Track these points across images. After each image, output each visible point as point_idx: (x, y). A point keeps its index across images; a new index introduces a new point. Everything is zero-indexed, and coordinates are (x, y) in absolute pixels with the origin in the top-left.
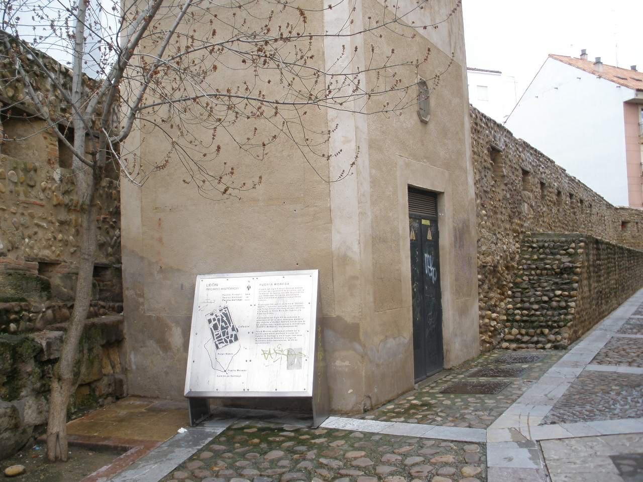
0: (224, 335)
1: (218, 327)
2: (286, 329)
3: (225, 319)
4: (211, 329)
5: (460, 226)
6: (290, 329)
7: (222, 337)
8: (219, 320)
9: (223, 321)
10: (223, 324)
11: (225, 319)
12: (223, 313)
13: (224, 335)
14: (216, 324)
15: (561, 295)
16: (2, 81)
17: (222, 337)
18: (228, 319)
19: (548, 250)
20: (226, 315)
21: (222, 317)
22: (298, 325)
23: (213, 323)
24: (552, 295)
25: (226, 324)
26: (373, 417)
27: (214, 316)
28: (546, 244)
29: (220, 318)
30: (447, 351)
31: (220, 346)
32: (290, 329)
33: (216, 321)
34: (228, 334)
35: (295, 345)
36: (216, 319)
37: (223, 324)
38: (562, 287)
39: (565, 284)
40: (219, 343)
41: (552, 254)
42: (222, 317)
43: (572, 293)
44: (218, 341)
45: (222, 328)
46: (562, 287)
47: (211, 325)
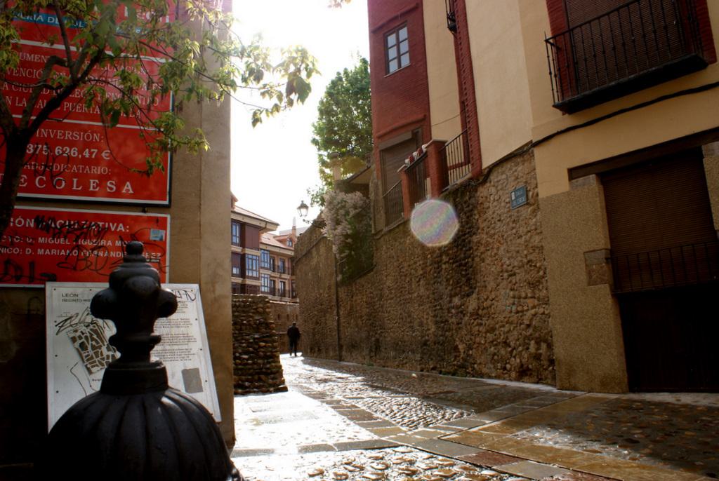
0: (97, 357)
1: (87, 347)
2: (175, 347)
3: (95, 336)
4: (77, 349)
5: (438, 230)
6: (180, 347)
7: (95, 359)
8: (86, 337)
9: (93, 339)
10: (94, 343)
11: (95, 336)
12: (91, 330)
13: (97, 357)
14: (83, 343)
15: (265, 346)
16: (339, 74)
17: (95, 359)
18: (98, 336)
19: (239, 309)
20: (96, 332)
21: (91, 335)
22: (189, 343)
23: (79, 341)
24: (257, 346)
25: (97, 343)
26: (699, 408)
27: (79, 334)
28: (237, 304)
29: (88, 335)
30: (617, 315)
31: (94, 370)
32: (180, 347)
33: (83, 340)
34: (102, 354)
35: (190, 365)
36: (83, 336)
37: (94, 343)
38: (264, 339)
39: (267, 336)
40: (92, 367)
41: (244, 312)
42: (91, 335)
43: (275, 344)
44: (90, 363)
45: (93, 347)
46: (264, 339)
47: (77, 344)
